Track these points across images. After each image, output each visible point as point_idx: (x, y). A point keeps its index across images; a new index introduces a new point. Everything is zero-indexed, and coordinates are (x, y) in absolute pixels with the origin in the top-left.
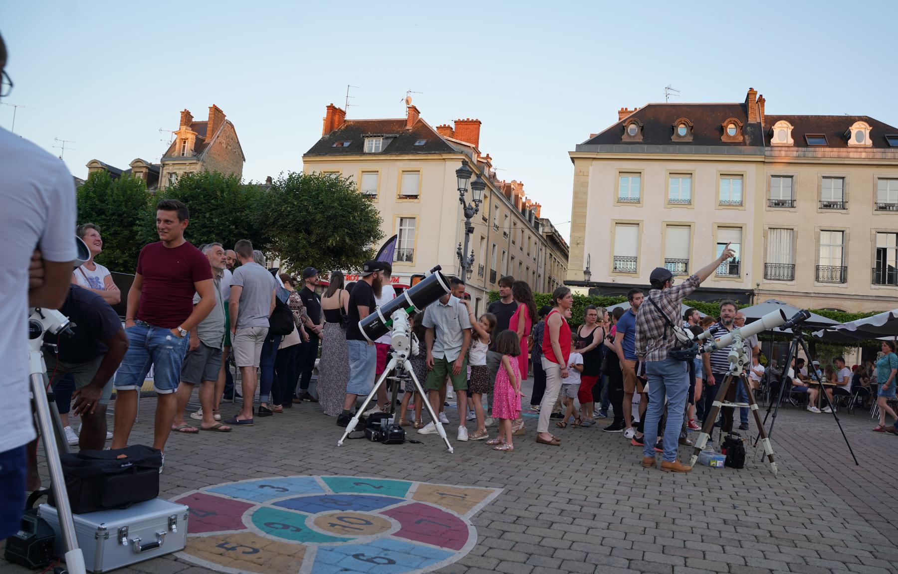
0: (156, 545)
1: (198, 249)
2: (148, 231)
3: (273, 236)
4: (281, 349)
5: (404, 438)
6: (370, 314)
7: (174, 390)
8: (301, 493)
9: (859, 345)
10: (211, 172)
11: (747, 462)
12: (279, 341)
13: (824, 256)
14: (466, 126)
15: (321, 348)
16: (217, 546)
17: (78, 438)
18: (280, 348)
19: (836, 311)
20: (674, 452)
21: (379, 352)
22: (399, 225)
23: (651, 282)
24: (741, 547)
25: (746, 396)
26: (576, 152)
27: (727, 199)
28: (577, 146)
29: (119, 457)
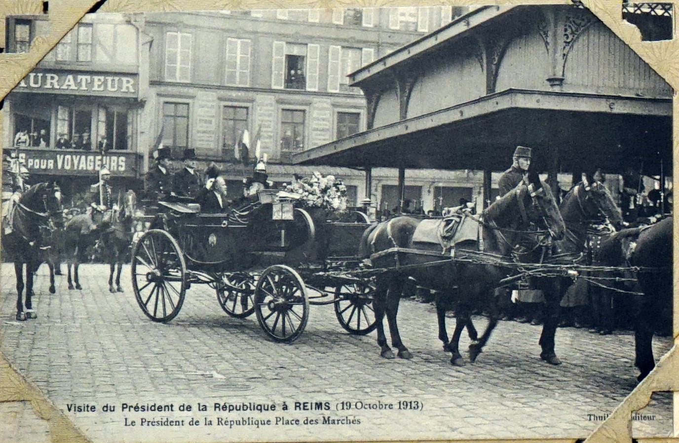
24: (172, 410)
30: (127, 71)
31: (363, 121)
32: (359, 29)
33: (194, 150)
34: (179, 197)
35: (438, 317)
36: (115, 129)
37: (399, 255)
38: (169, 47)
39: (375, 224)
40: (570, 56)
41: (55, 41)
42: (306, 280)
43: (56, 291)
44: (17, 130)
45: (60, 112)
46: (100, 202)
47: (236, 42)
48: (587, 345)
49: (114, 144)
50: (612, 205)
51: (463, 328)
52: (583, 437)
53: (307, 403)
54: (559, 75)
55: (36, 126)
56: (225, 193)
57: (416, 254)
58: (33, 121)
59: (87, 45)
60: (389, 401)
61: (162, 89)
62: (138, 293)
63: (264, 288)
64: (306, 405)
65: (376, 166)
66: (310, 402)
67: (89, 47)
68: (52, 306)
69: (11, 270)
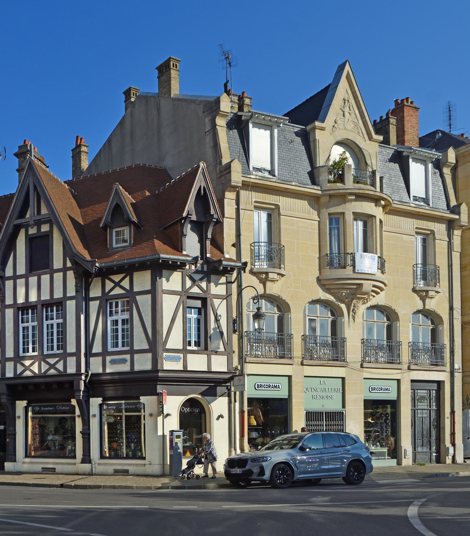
0: (405, 458)
1: (391, 117)
2: (428, 348)
3: (278, 474)
6: (257, 476)
7: (182, 475)
10: (313, 299)
12: (382, 119)
13: (420, 263)
14: (200, 509)
15: (148, 165)
16: (201, 185)
17: (175, 273)
18: (129, 276)
20: (393, 181)
22: (46, 330)
23: (453, 206)
24: (419, 109)
26: (396, 458)
29: (183, 223)
30: (150, 473)
33: (420, 138)
34: (82, 389)
35: (47, 231)
36: (52, 506)
42: (104, 270)
44: (106, 269)
46: (227, 115)
47: (377, 320)
51: (105, 281)
52: (346, 184)
61: (373, 264)
67: (418, 263)
68: (365, 450)
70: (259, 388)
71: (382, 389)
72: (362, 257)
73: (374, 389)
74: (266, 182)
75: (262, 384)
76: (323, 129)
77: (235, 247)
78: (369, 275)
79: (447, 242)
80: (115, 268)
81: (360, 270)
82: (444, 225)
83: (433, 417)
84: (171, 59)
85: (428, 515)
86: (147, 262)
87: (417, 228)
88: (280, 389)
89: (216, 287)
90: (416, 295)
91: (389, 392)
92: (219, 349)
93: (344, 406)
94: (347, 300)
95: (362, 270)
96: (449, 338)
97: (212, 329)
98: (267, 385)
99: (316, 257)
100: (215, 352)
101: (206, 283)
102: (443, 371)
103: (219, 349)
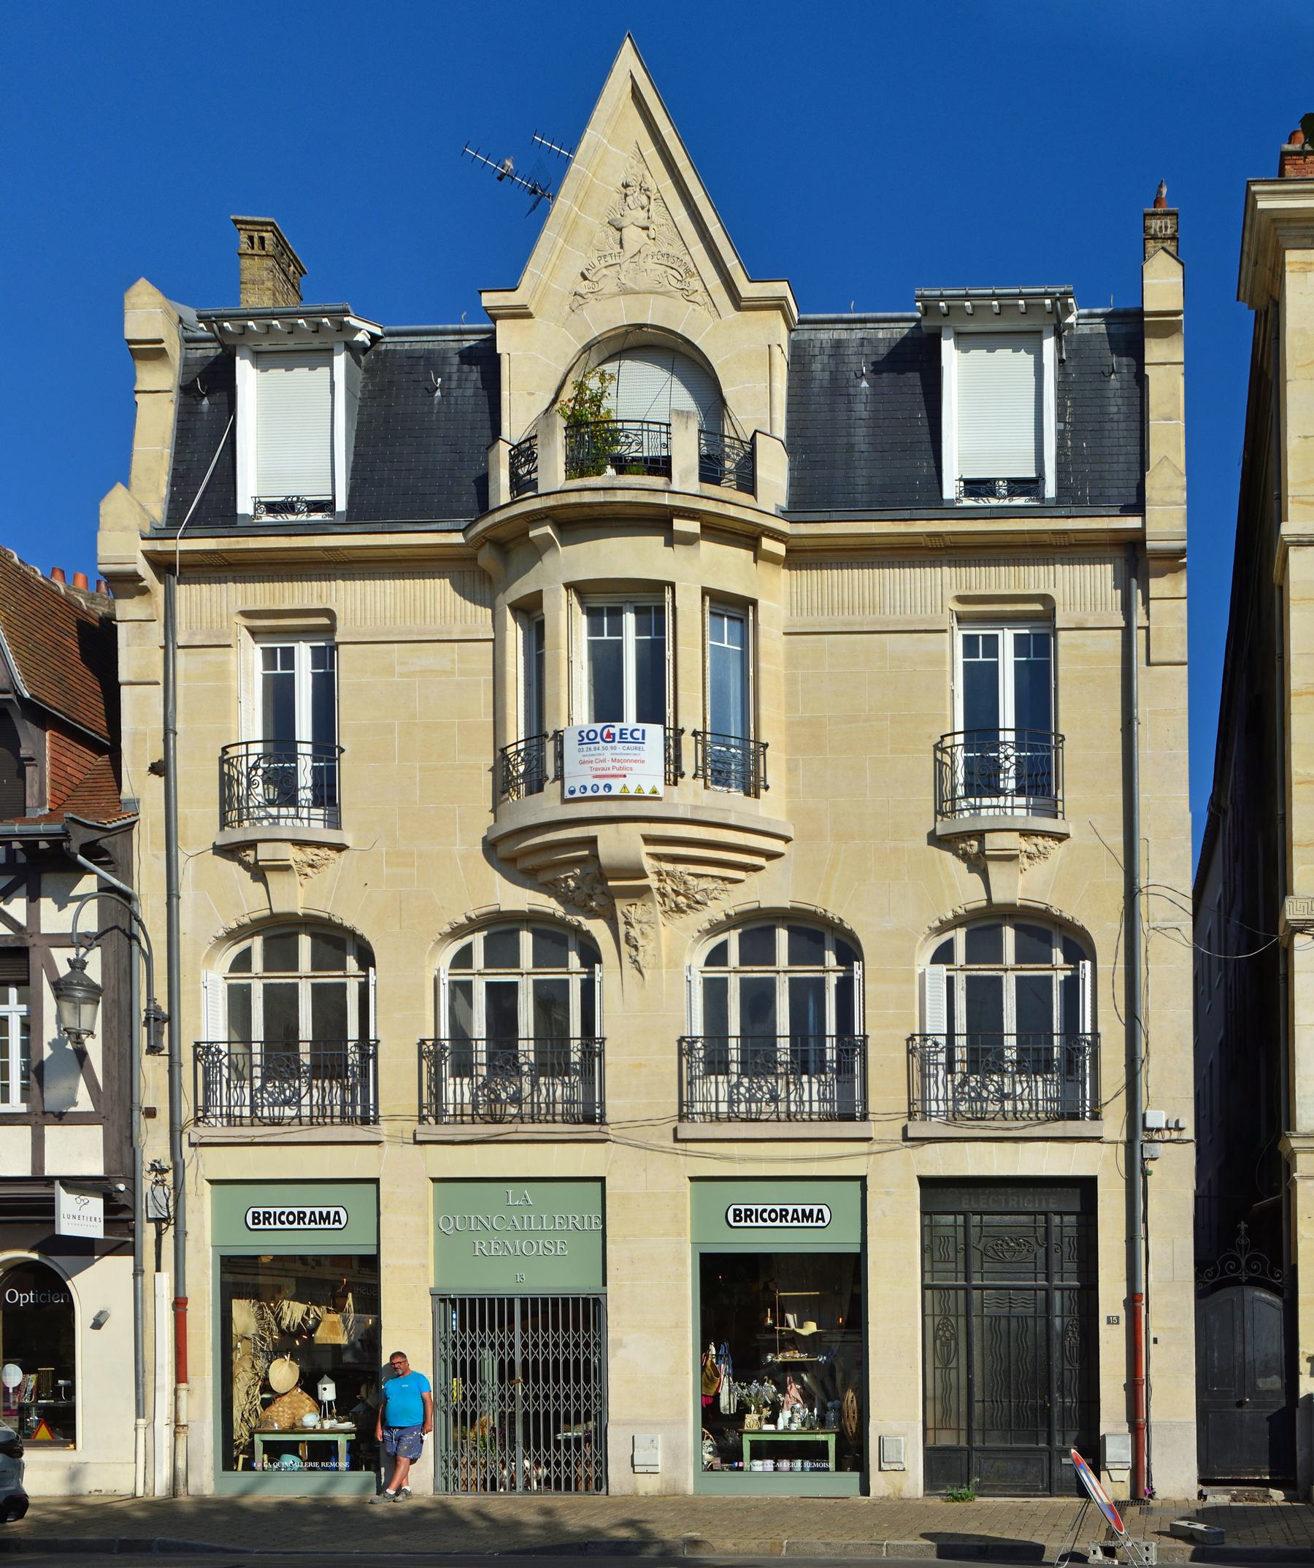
4: (621, 43)
5: (757, 1075)
7: (1003, 1106)
8: (94, 1018)
9: (513, 1051)
11: (32, 904)
19: (1244, 1279)
21: (653, 1551)
25: (285, 1095)
27: (1154, 1418)
28: (87, 963)
31: (735, 720)
32: (121, 1142)
37: (568, 1063)
38: (661, 466)
39: (762, 1052)
40: (644, 233)
41: (690, 251)
43: (1038, 1540)
45: (1051, 1200)
48: (109, 970)
49: (734, 1055)
50: (1084, 1102)
53: (627, 730)
54: (871, 1117)
55: (310, 1261)
56: (108, 736)
57: (212, 1510)
58: (1011, 1055)
59: (1035, 1222)
60: (654, 214)
62: (224, 814)
63: (779, 1296)
64: (624, 732)
65: (825, 1032)
66: (345, 836)
69: (410, 1447)
70: (740, 1221)
71: (303, 1219)
72: (586, 741)
73: (265, 1218)
74: (238, 542)
75: (272, 1210)
76: (522, 313)
77: (161, 776)
78: (610, 803)
79: (1119, 632)
80: (43, 845)
81: (577, 791)
82: (1109, 568)
83: (1062, 1317)
84: (1254, 188)
85: (1007, 715)
86: (786, 514)
87: (961, 599)
88: (824, 1224)
89: (60, 910)
90: (948, 856)
91: (337, 1225)
92: (75, 1104)
93: (605, 1284)
94: (594, 903)
95: (585, 788)
96: (1122, 1010)
97: (49, 1044)
98: (291, 1213)
99: (480, 768)
100: (56, 1117)
101: (24, 901)
102: (1097, 1139)
103: (75, 1104)
